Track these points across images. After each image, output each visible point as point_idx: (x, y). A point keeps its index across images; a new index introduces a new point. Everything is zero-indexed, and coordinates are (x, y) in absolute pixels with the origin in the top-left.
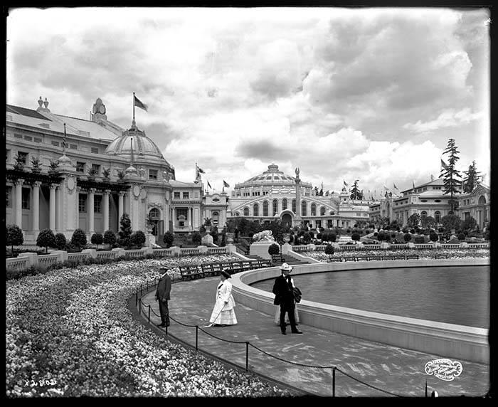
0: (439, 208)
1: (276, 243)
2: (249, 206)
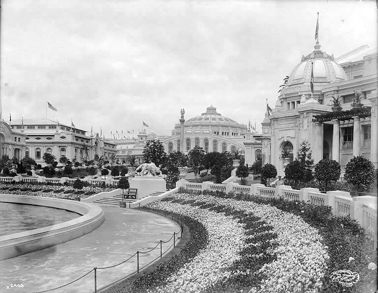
1: (234, 172)
2: (173, 141)
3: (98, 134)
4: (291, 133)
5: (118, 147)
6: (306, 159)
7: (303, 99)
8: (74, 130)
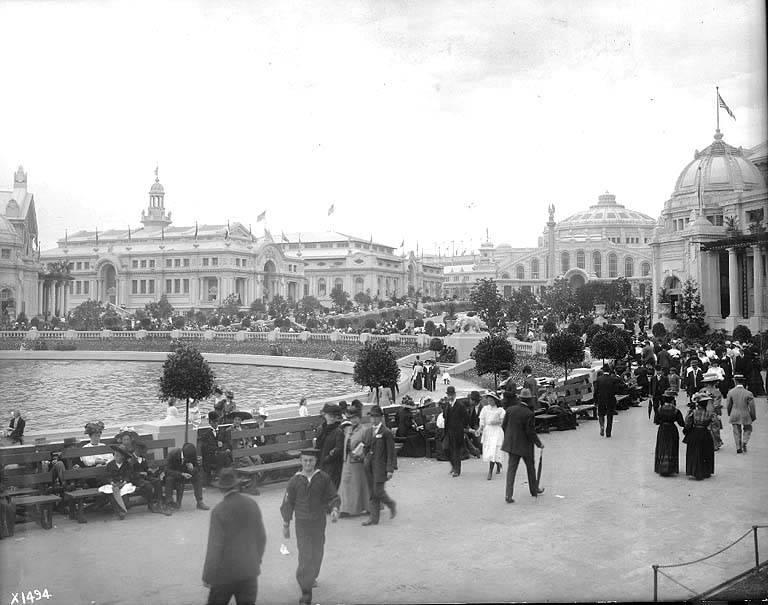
2: (524, 263)
3: (412, 253)
4: (678, 265)
5: (447, 270)
6: (693, 304)
8: (376, 247)
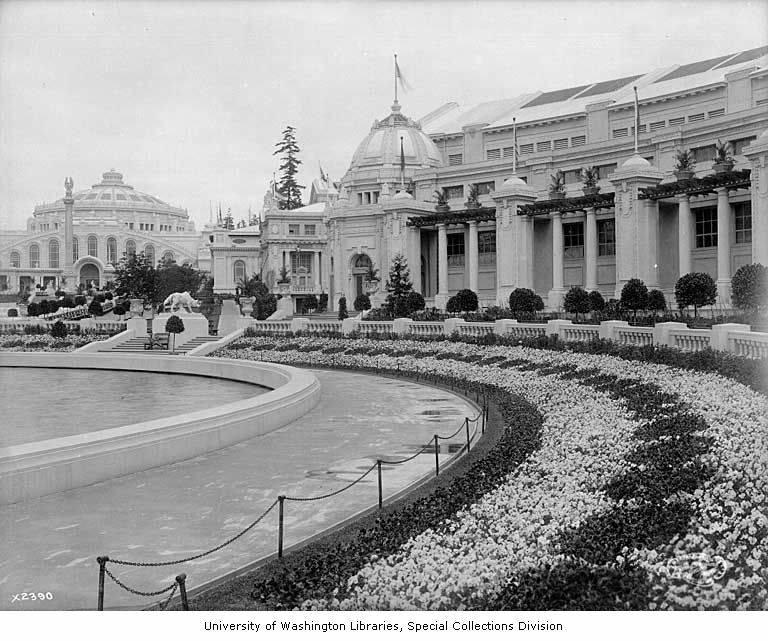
0: (242, 253)
4: (369, 242)
7: (385, 189)
